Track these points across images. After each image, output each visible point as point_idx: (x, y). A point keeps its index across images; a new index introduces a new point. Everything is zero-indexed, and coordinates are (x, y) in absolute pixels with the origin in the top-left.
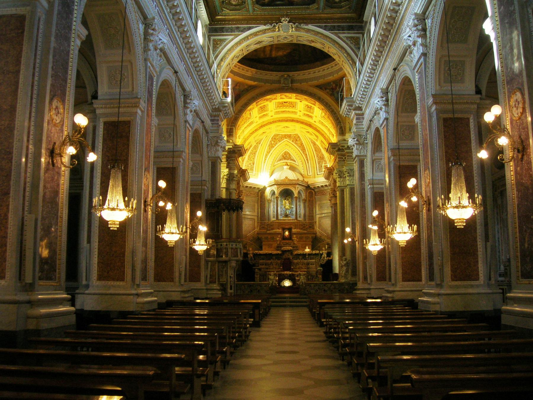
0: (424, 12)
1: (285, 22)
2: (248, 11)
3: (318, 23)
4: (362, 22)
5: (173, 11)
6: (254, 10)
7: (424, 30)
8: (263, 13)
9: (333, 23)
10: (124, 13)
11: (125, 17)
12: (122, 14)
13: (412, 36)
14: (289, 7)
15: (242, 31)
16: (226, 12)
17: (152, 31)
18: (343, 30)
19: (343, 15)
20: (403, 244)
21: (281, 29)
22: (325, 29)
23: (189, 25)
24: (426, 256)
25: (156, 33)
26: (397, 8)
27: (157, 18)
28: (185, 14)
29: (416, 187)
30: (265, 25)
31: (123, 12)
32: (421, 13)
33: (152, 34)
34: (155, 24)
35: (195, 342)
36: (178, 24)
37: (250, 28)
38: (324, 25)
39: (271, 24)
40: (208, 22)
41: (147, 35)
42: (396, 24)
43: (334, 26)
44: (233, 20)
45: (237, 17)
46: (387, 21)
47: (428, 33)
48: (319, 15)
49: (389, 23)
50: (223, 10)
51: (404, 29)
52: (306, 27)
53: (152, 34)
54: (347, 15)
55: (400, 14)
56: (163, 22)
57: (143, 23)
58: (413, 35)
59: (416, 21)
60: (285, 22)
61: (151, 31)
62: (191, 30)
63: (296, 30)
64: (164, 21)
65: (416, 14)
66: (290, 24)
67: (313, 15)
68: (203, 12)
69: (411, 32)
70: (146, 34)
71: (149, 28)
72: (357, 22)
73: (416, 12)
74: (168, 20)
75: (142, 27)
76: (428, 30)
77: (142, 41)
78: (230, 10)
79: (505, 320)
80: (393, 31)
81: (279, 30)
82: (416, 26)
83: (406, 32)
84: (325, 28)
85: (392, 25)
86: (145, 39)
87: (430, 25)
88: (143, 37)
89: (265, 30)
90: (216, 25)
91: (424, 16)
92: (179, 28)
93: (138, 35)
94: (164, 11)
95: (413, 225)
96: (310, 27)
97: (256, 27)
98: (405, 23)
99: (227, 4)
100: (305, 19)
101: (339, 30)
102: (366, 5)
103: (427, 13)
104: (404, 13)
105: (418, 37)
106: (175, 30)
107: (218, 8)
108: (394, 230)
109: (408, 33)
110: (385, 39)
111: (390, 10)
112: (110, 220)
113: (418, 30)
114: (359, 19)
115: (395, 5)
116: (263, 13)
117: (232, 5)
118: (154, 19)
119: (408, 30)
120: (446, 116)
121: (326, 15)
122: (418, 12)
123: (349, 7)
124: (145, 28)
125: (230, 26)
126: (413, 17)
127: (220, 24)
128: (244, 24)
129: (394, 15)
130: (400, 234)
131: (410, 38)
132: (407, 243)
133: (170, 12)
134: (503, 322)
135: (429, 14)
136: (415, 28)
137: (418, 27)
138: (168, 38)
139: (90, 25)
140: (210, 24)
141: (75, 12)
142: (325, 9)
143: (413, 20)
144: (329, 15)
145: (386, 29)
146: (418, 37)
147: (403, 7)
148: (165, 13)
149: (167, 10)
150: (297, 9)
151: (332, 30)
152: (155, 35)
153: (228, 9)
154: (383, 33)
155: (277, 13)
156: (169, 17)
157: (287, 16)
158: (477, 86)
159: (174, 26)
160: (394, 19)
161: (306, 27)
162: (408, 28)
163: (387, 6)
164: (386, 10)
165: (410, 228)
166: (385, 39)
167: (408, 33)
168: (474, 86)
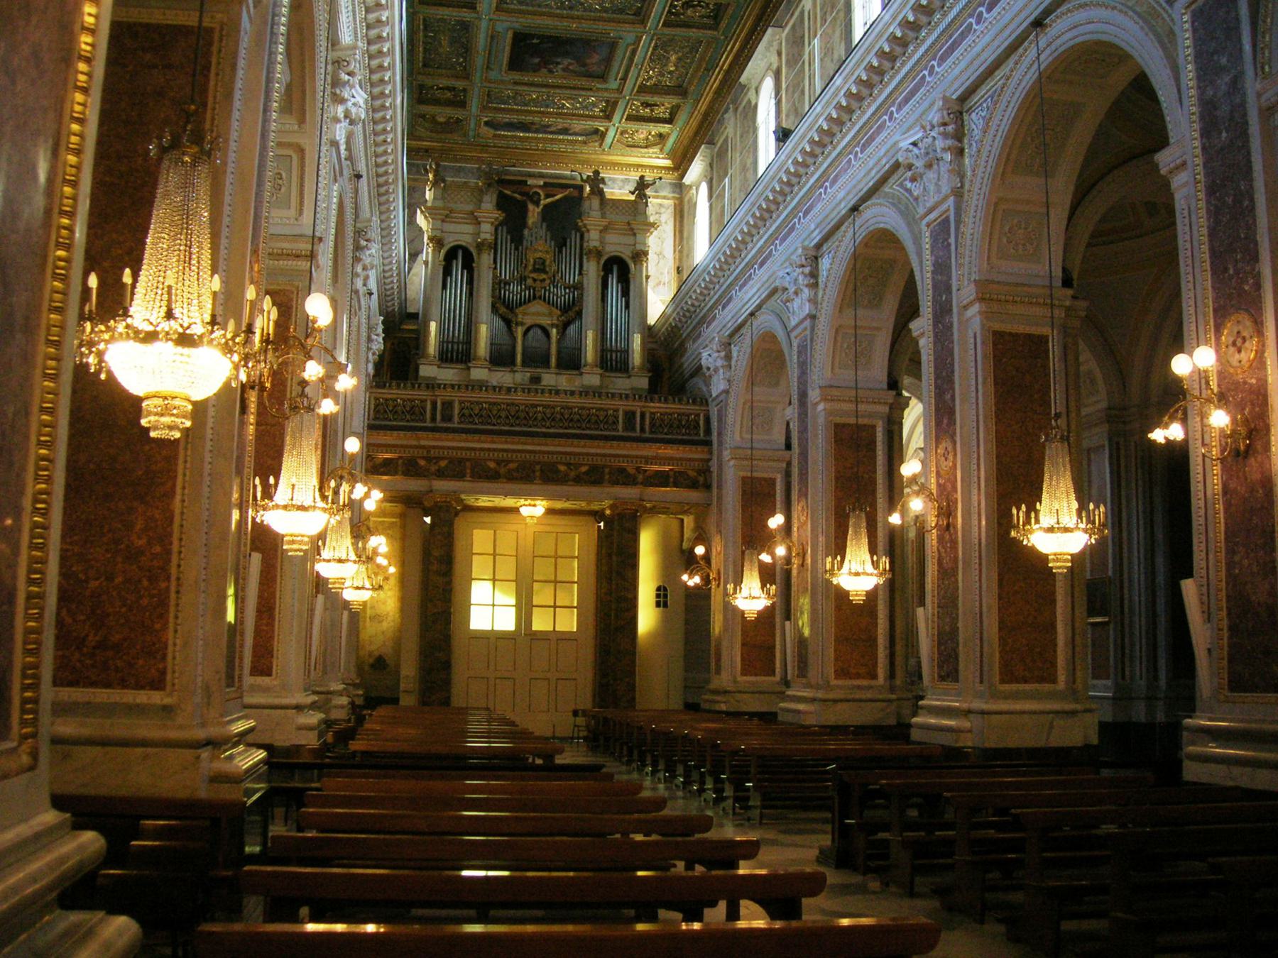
20: (751, 616)
24: (933, 615)
29: (707, 558)
32: (954, 97)
35: (465, 873)
79: (915, 735)
95: (1091, 506)
108: (1033, 520)
112: (152, 389)
113: (945, 135)
120: (839, 420)
130: (1050, 535)
132: (1072, 561)
134: (1192, 772)
158: (890, 374)
165: (1084, 514)
168: (886, 374)
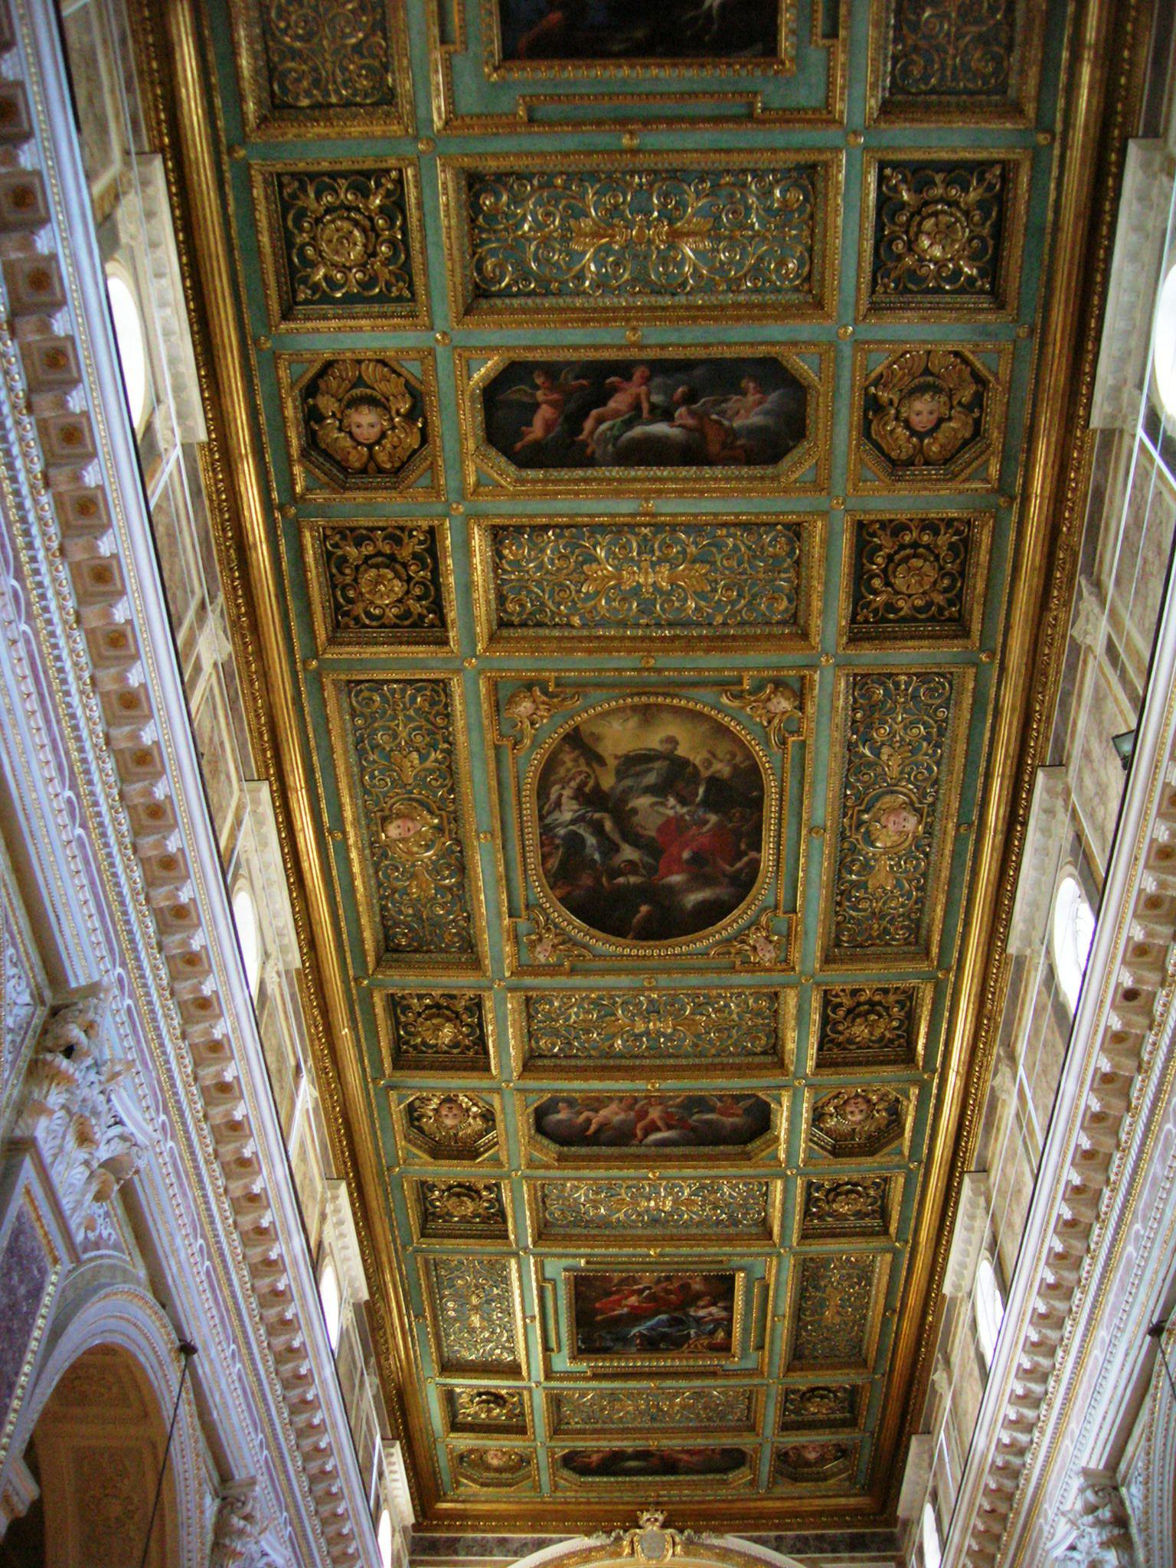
0: (1113, 1465)
1: (651, 1524)
2: (537, 1487)
3: (757, 1528)
4: (892, 1520)
5: (314, 1467)
6: (556, 1487)
7: (1121, 1521)
8: (583, 1496)
9: (800, 1527)
10: (161, 1458)
11: (163, 1468)
12: (156, 1457)
13: (1082, 1545)
14: (665, 1478)
15: (516, 1554)
16: (470, 1491)
17: (242, 1523)
18: (834, 1551)
19: (833, 1501)
21: (638, 1548)
22: (777, 1549)
23: (352, 1499)
25: (256, 1530)
26: (1016, 1461)
27: (263, 1480)
28: (348, 1481)
30: (588, 1533)
31: (161, 1449)
33: (241, 1532)
34: (255, 1499)
36: (325, 1510)
37: (540, 1545)
38: (773, 1534)
39: (608, 1533)
40: (410, 1519)
41: (225, 1535)
42: (1017, 1513)
43: (806, 1538)
44: (488, 1516)
45: (503, 1506)
46: (987, 1507)
47: (1134, 1530)
48: (759, 1504)
49: (993, 1511)
50: (458, 1483)
51: (1046, 1528)
52: (716, 1542)
53: (241, 1532)
54: (843, 1501)
55: (1027, 1480)
56: (278, 1499)
57: (216, 1494)
58: (1086, 1540)
59: (1090, 1495)
60: (651, 1524)
61: (237, 1522)
62: (362, 1534)
63: (687, 1553)
64: (286, 1500)
65: (1086, 1472)
66: (670, 1531)
67: (738, 1505)
68: (398, 1484)
69: (1075, 1533)
70: (222, 1529)
71: (232, 1512)
72: (874, 1524)
73: (1083, 1463)
74: (292, 1492)
75: (211, 1505)
76: (1133, 1523)
77: (208, 1551)
78: (483, 1485)
80: (1010, 1536)
81: (633, 1553)
82: (1091, 1509)
83: (1057, 1538)
84: (778, 1545)
85: (1005, 1518)
86: (217, 1545)
87: (1136, 1502)
88: (210, 1538)
89: (590, 1550)
90: (436, 1528)
91: (1113, 1477)
92: (324, 1522)
93: (195, 1529)
94: (285, 1466)
96: (732, 1541)
97: (561, 1540)
98: (1049, 1508)
99: (473, 1465)
100: (713, 1517)
101: (822, 1551)
102: (903, 1469)
103: (1123, 1466)
104: (1041, 1476)
105: (1104, 1545)
106: (314, 1531)
107: (446, 1477)
109: (1065, 1537)
110: (990, 1548)
111: (996, 1470)
113: (1099, 1523)
114: (882, 1512)
115: (1030, 1380)
116: (583, 1496)
117: (488, 1468)
118: (253, 1482)
119: (1062, 1527)
121: (778, 1504)
122: (1092, 1465)
123: (850, 1478)
124: (220, 1511)
125: (479, 1535)
126: (1077, 1482)
127: (449, 1528)
128: (522, 1531)
129: (1008, 1484)
131: (1075, 1554)
133: (291, 1423)
135: (1128, 1467)
136: (1090, 1518)
137: (1099, 1512)
138: (289, 1553)
139: (44, 1466)
140: (417, 1527)
141: (12, 1416)
142: (775, 1483)
143: (1082, 1490)
144: (787, 1504)
145: (986, 1531)
146: (1104, 1545)
147: (1035, 1458)
148: (286, 1472)
149: (293, 1459)
150: (689, 1484)
151: (799, 1552)
152: (250, 1535)
153: (474, 1481)
154: (976, 1547)
155: (627, 1497)
156: (299, 1485)
157: (658, 1505)
159: (310, 1517)
160: (1010, 1497)
161: (716, 1542)
162: (1063, 1520)
163: (984, 1456)
164: (993, 1422)
166: (990, 1548)
167: (1065, 1537)
